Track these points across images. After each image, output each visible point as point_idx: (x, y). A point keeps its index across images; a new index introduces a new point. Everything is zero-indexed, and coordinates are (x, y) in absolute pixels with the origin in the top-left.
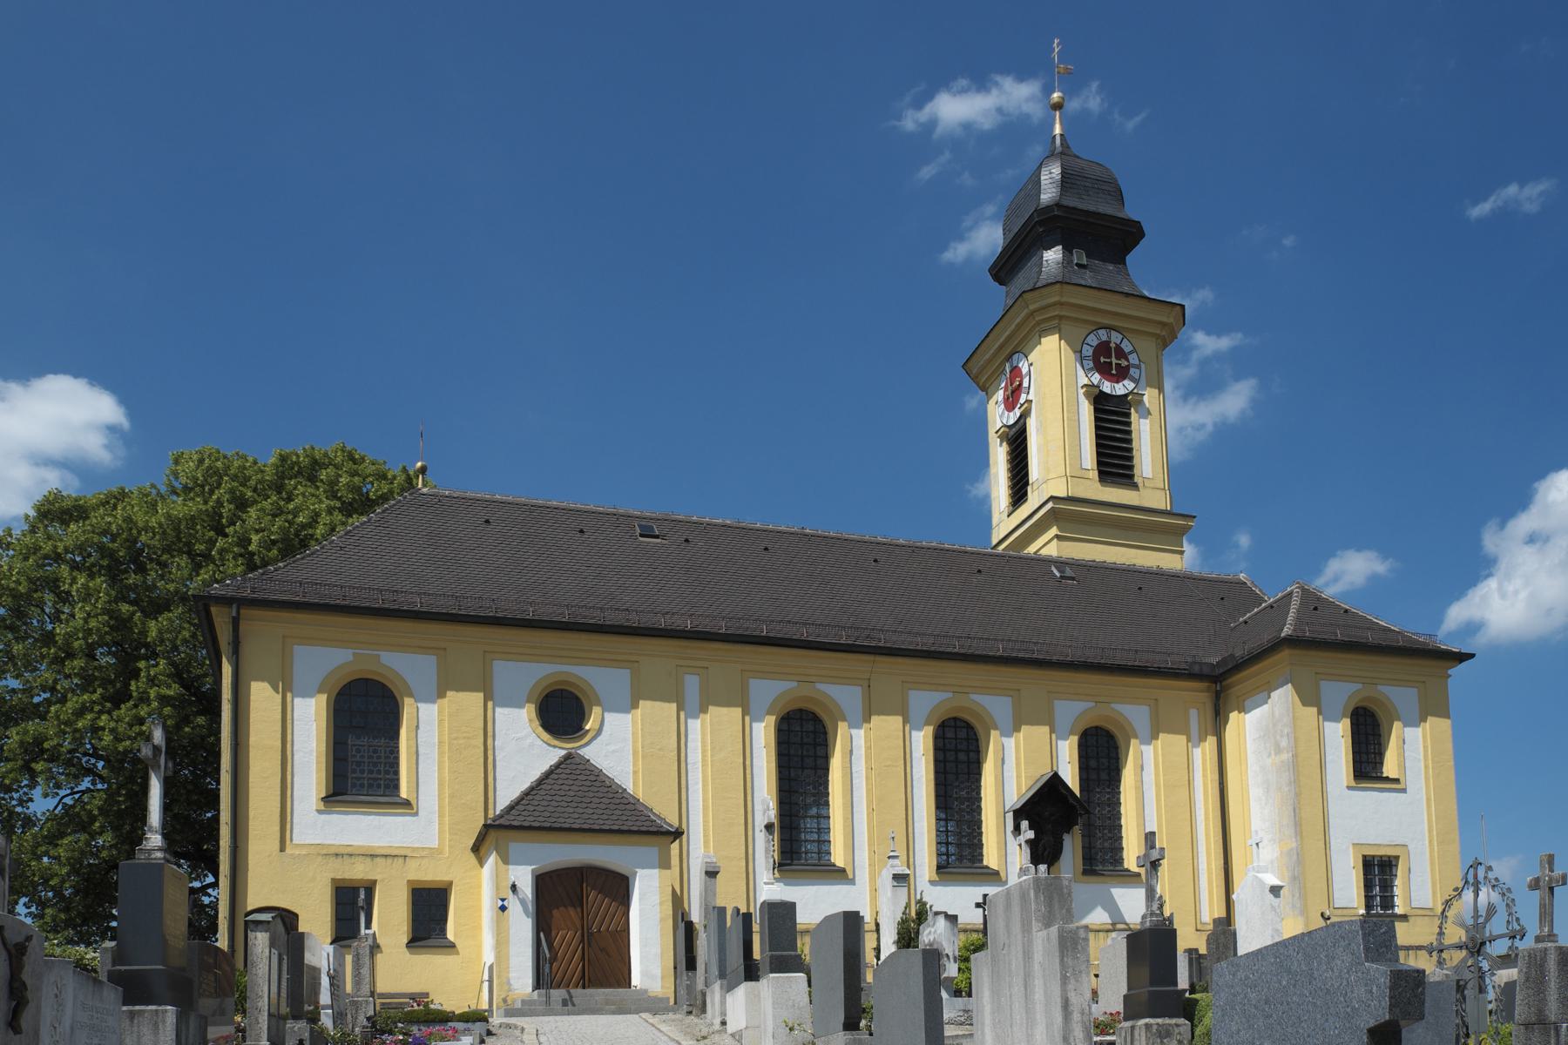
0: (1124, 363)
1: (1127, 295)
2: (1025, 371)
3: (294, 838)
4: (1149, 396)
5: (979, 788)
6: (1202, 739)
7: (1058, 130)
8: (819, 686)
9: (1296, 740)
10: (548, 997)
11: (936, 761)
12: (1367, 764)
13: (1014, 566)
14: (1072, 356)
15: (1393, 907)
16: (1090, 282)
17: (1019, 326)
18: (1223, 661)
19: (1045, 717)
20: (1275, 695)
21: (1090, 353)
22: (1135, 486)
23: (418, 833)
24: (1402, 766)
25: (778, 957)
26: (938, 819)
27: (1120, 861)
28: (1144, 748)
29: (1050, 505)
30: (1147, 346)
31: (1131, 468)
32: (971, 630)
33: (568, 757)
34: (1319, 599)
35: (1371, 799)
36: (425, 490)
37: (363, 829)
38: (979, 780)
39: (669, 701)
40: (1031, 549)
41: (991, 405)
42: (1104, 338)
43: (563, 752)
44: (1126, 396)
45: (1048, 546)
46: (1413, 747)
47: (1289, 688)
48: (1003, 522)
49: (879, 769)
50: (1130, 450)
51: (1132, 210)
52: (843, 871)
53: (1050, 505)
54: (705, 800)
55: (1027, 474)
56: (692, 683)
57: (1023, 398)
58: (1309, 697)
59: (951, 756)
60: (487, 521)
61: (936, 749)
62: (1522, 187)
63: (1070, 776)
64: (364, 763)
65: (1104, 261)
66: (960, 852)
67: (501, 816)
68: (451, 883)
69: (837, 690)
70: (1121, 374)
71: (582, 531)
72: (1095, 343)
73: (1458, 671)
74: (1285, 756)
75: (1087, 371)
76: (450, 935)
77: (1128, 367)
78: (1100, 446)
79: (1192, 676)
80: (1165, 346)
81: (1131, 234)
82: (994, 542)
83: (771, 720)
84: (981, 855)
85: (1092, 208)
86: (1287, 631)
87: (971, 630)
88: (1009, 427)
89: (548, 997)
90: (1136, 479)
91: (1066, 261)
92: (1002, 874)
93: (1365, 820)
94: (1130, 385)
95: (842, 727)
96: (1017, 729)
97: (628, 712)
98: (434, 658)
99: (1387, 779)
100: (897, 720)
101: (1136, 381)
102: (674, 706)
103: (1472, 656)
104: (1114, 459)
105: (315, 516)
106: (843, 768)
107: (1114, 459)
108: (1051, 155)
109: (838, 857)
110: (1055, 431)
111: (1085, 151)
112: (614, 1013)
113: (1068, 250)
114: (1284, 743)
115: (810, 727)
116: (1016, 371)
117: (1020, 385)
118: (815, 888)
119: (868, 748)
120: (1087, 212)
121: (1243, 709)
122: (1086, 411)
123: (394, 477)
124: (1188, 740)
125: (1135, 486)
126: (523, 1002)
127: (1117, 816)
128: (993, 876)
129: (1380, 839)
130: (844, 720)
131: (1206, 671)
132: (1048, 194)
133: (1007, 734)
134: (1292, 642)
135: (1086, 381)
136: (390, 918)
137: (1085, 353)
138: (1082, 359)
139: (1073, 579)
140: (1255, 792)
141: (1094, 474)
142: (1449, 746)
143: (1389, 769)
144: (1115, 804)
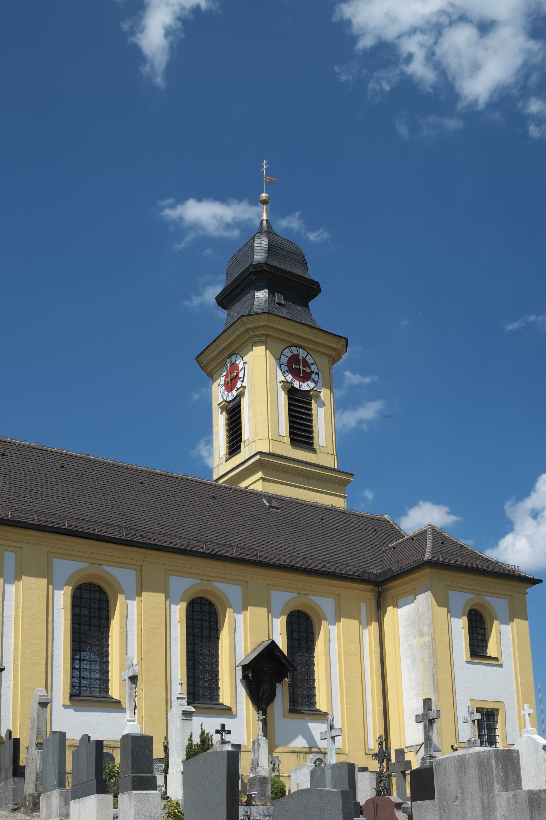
0: (308, 370)
1: (311, 327)
2: (241, 366)
4: (325, 394)
5: (107, 637)
6: (369, 624)
8: (105, 568)
9: (434, 628)
11: (187, 627)
12: (478, 648)
13: (228, 497)
16: (286, 315)
17: (238, 337)
18: (383, 573)
19: (264, 602)
20: (420, 597)
21: (286, 360)
22: (314, 451)
24: (500, 650)
25: (139, 778)
27: (313, 704)
28: (331, 627)
29: (258, 457)
31: (312, 438)
32: (213, 538)
34: (444, 537)
35: (480, 670)
38: (217, 642)
39: (265, 607)
40: (243, 485)
41: (215, 386)
42: (295, 352)
44: (309, 391)
45: (255, 483)
46: (505, 637)
47: (429, 594)
49: (146, 629)
50: (311, 427)
51: (313, 274)
53: (258, 457)
54: (16, 645)
55: (240, 434)
57: (239, 384)
58: (442, 601)
61: (188, 618)
63: (282, 643)
70: (306, 377)
72: (289, 355)
74: (427, 639)
75: (283, 373)
77: (310, 373)
78: (291, 422)
79: (363, 581)
81: (311, 289)
83: (69, 589)
85: (288, 269)
86: (427, 556)
87: (213, 538)
88: (229, 402)
90: (315, 446)
91: (271, 300)
92: (234, 710)
93: (477, 684)
95: (121, 598)
96: (245, 608)
98: (240, 588)
99: (490, 658)
100: (161, 597)
101: (316, 383)
104: (301, 431)
106: (121, 628)
107: (301, 431)
108: (261, 232)
110: (262, 408)
113: (272, 293)
114: (426, 630)
115: (97, 595)
116: (234, 366)
117: (237, 375)
118: (97, 714)
119: (140, 615)
121: (396, 605)
122: (283, 398)
124: (360, 624)
125: (314, 451)
127: (312, 673)
128: (227, 711)
129: (488, 696)
130: (122, 593)
131: (372, 578)
132: (259, 256)
133: (238, 611)
134: (432, 564)
135: (283, 379)
138: (280, 364)
139: (278, 508)
140: (405, 662)
141: (288, 440)
142: (528, 638)
143: (491, 651)
144: (310, 664)
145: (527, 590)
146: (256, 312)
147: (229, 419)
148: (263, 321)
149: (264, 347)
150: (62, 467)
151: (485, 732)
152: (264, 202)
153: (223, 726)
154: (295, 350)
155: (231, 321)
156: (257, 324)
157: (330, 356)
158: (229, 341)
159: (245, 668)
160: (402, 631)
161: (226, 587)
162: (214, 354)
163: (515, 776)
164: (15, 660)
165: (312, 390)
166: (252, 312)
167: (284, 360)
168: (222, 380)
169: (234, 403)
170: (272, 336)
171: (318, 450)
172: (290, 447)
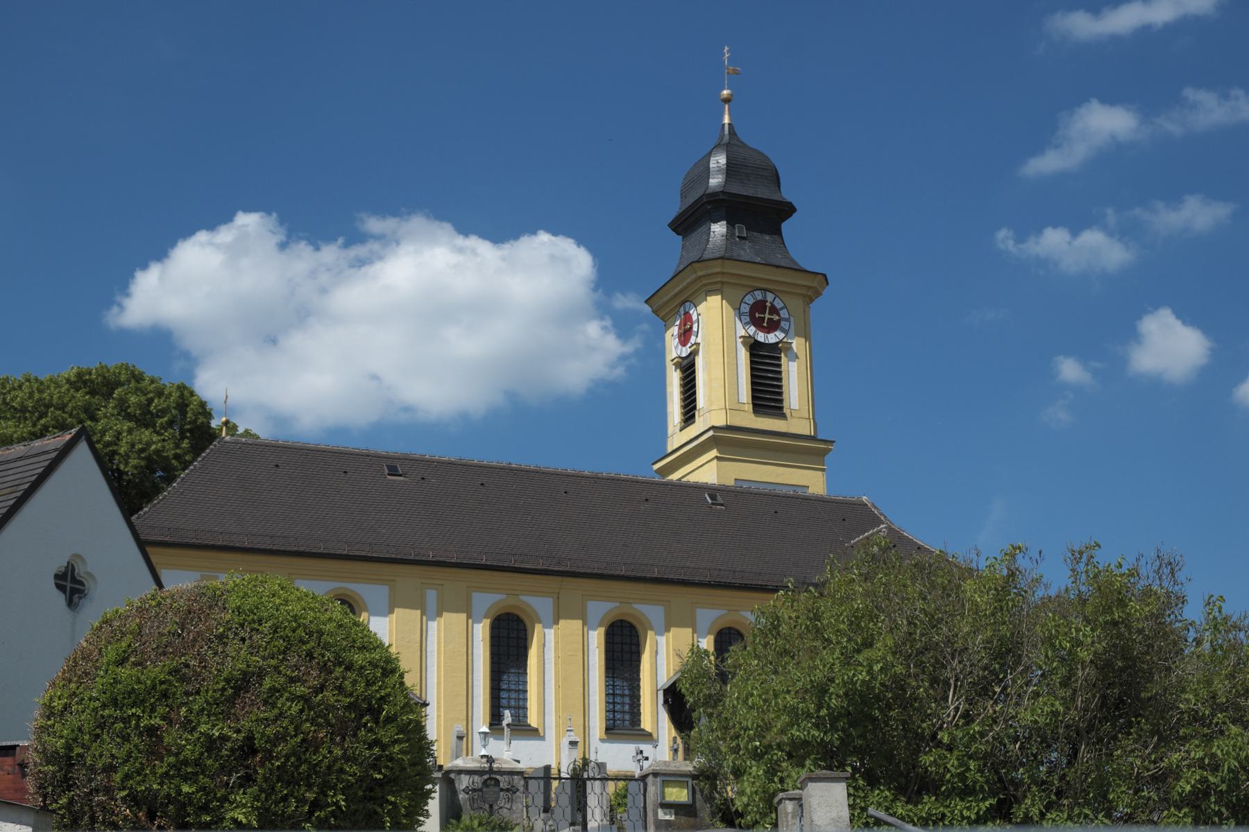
0: (776, 318)
2: (694, 317)
4: (798, 344)
5: (638, 671)
7: (726, 120)
8: (522, 598)
11: (607, 651)
14: (732, 312)
22: (783, 416)
29: (711, 433)
30: (795, 304)
31: (781, 401)
36: (228, 438)
38: (639, 666)
41: (668, 335)
44: (777, 343)
48: (677, 438)
49: (564, 657)
51: (788, 193)
52: (537, 730)
53: (711, 433)
54: (439, 678)
55: (695, 400)
56: (432, 596)
59: (617, 639)
62: (1075, 233)
65: (761, 232)
66: (623, 721)
69: (534, 600)
70: (772, 327)
72: (751, 302)
75: (745, 324)
77: (779, 321)
80: (812, 300)
81: (788, 210)
82: (670, 450)
83: (487, 622)
84: (640, 720)
91: (729, 236)
92: (655, 736)
94: (780, 335)
96: (667, 630)
97: (385, 615)
101: (786, 332)
102: (419, 612)
104: (767, 394)
105: (118, 435)
107: (767, 394)
109: (533, 720)
110: (718, 372)
111: (751, 139)
113: (731, 224)
116: (688, 317)
119: (557, 643)
120: (748, 197)
122: (743, 356)
123: (170, 394)
125: (783, 416)
128: (648, 737)
132: (715, 181)
135: (743, 333)
137: (742, 310)
138: (740, 315)
146: (711, 256)
147: (683, 379)
148: (717, 268)
149: (719, 297)
154: (759, 296)
155: (682, 267)
156: (710, 271)
157: (805, 296)
158: (676, 290)
161: (648, 610)
162: (665, 299)
164: (439, 693)
165: (781, 341)
166: (706, 256)
167: (745, 309)
168: (675, 330)
170: (728, 283)
171: (788, 415)
172: (753, 416)
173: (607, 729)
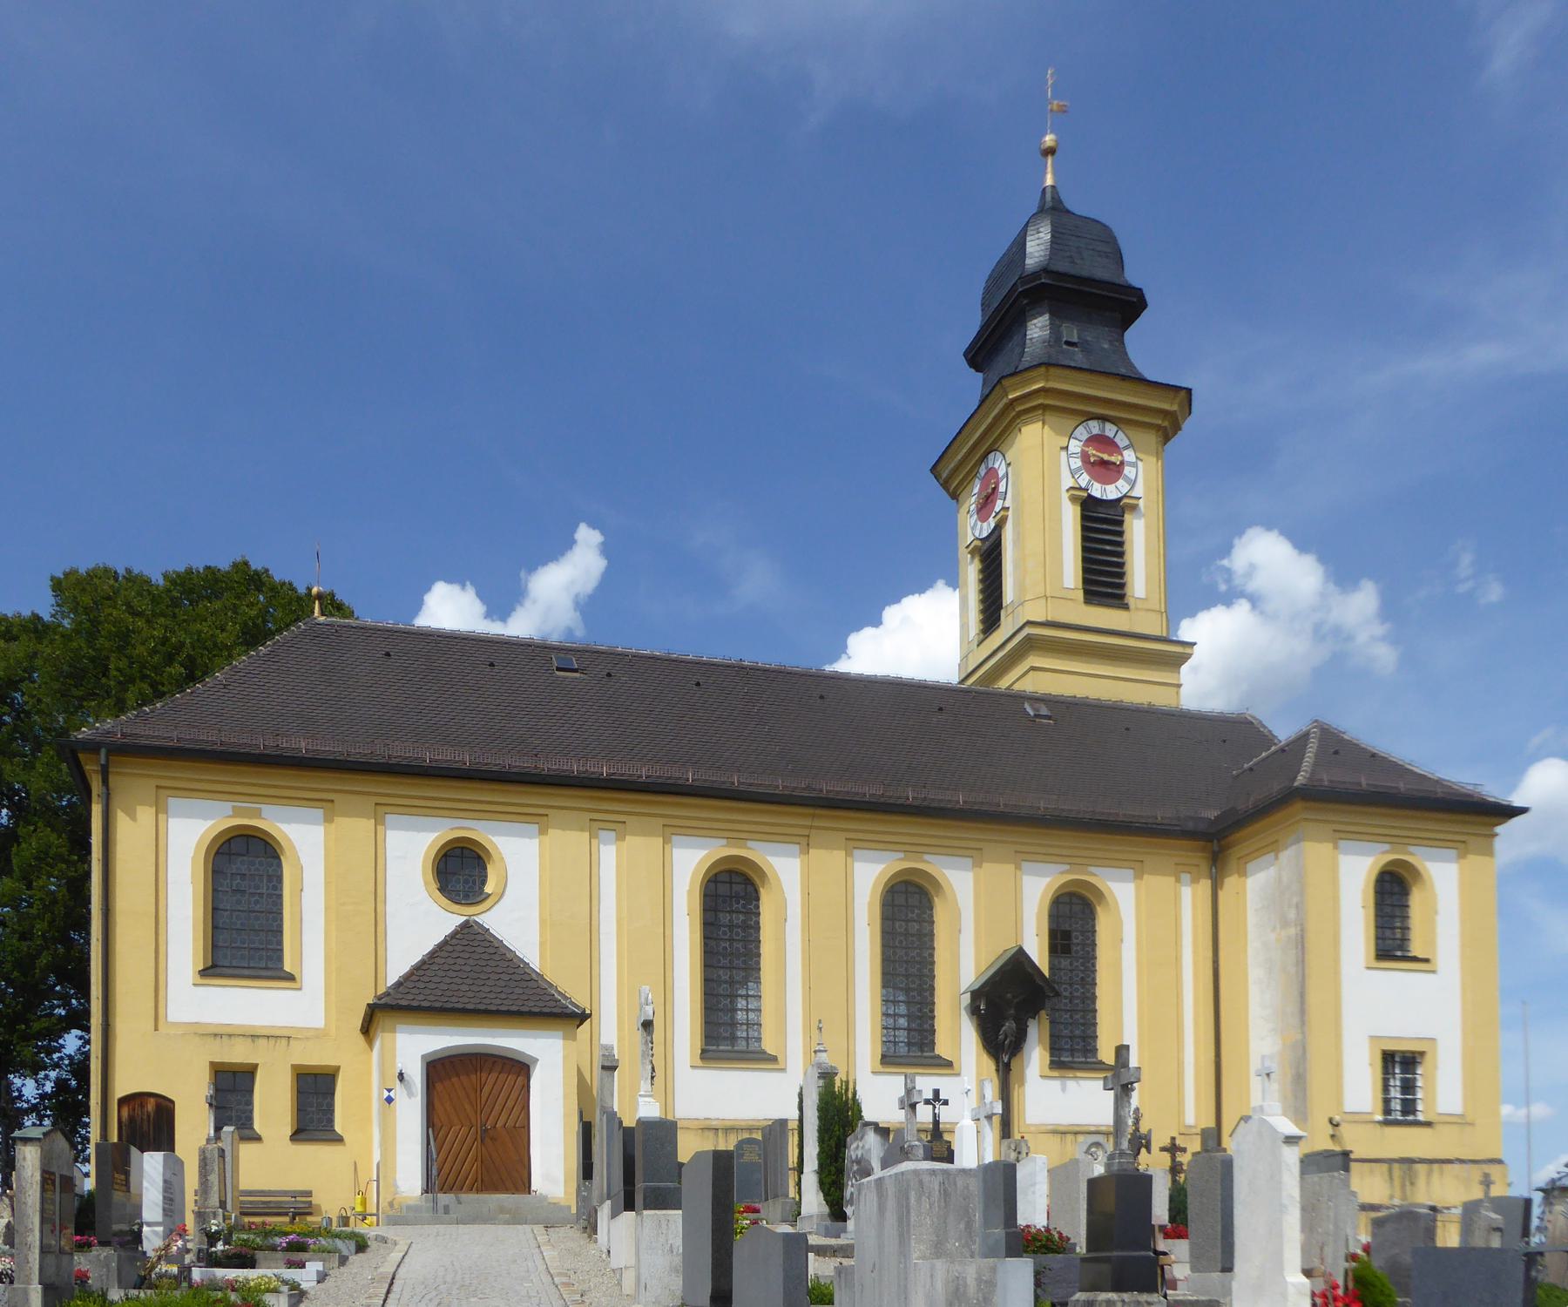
2: (1001, 473)
3: (165, 1011)
7: (1049, 181)
10: (435, 1201)
15: (1414, 1112)
23: (294, 1013)
25: (654, 1189)
26: (886, 1001)
27: (1094, 1051)
29: (792, 1193)
31: (1122, 586)
33: (466, 926)
35: (1395, 978)
37: (244, 1005)
40: (1003, 684)
43: (464, 919)
44: (1119, 500)
51: (1134, 275)
53: (1027, 631)
57: (999, 505)
60: (388, 654)
63: (1038, 951)
64: (244, 930)
66: (911, 1043)
67: (387, 994)
68: (338, 1068)
71: (492, 665)
73: (1505, 830)
74: (1292, 931)
76: (338, 1128)
86: (1301, 779)
89: (435, 1201)
91: (1055, 337)
99: (1415, 959)
103: (1523, 811)
112: (507, 1223)
116: (992, 472)
117: (994, 489)
122: (1070, 518)
125: (1126, 607)
126: (409, 1208)
129: (1403, 1031)
135: (1071, 483)
136: (273, 1104)
139: (1049, 718)
141: (1080, 594)
145: (1498, 829)
150: (698, 684)
151: (1395, 1093)
152: (1051, 151)
153: (936, 1092)
159: (976, 995)
160: (1252, 919)
163: (962, 1226)
165: (1125, 496)
169: (992, 540)
173: (884, 1056)
